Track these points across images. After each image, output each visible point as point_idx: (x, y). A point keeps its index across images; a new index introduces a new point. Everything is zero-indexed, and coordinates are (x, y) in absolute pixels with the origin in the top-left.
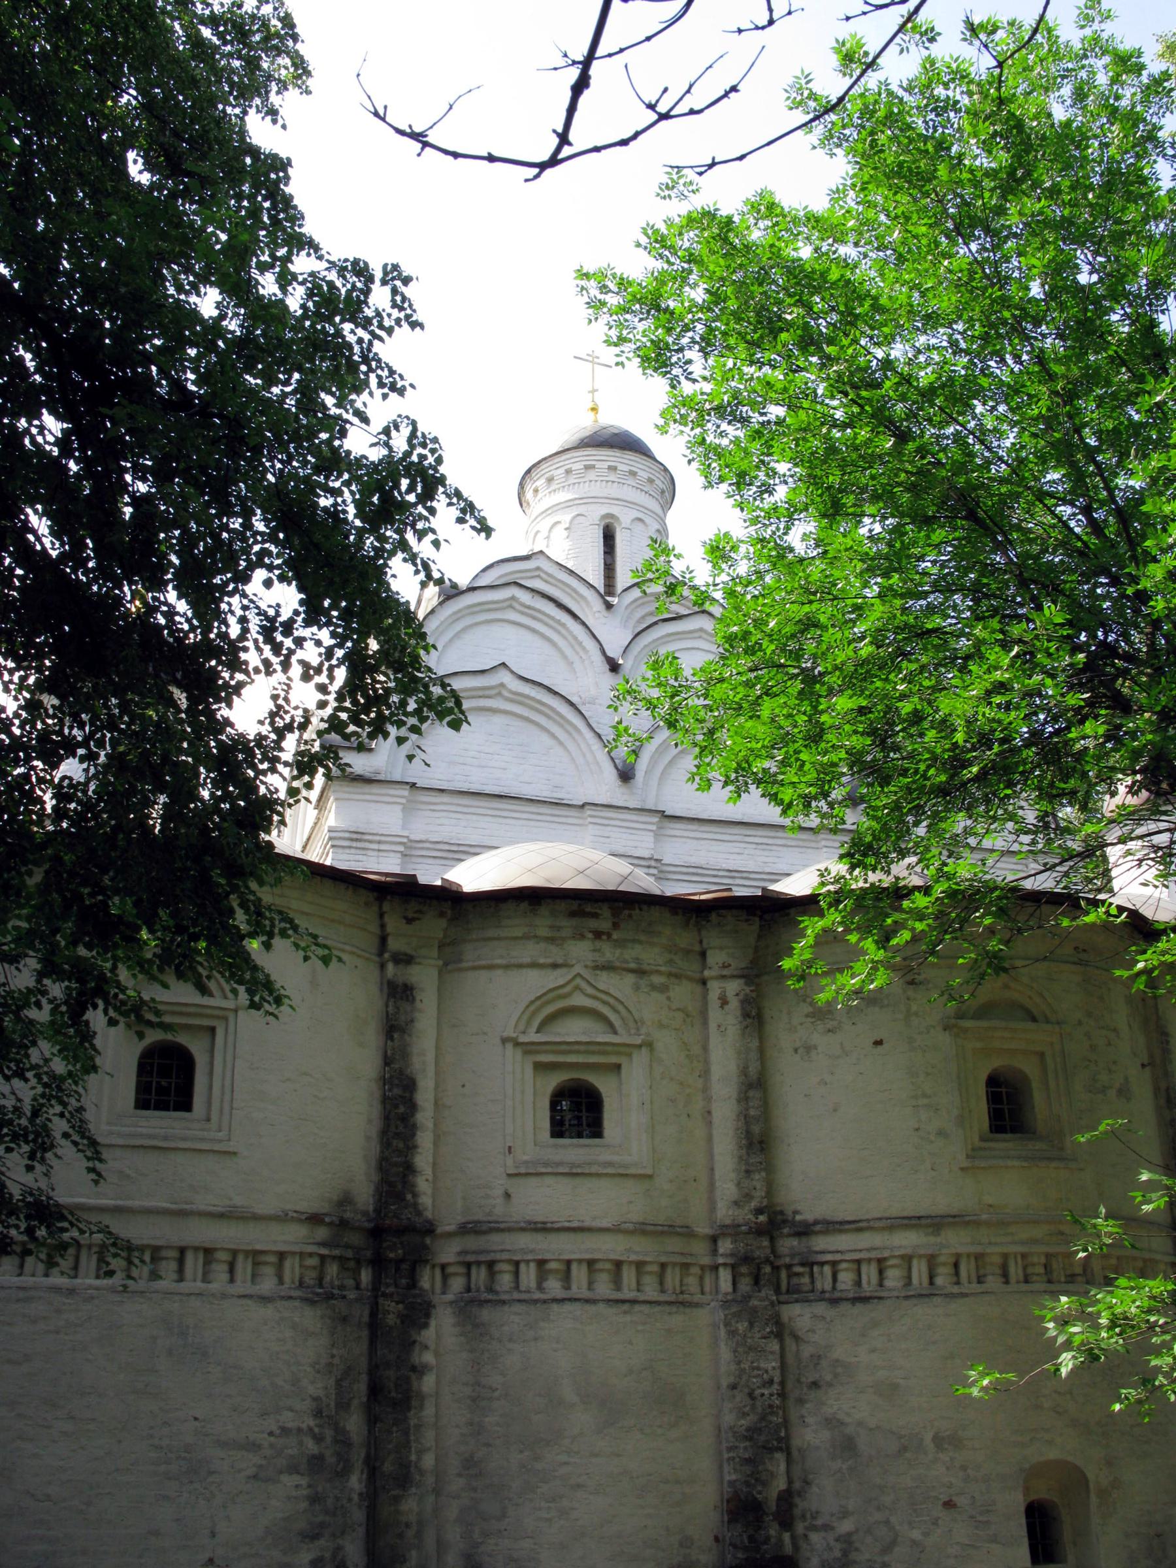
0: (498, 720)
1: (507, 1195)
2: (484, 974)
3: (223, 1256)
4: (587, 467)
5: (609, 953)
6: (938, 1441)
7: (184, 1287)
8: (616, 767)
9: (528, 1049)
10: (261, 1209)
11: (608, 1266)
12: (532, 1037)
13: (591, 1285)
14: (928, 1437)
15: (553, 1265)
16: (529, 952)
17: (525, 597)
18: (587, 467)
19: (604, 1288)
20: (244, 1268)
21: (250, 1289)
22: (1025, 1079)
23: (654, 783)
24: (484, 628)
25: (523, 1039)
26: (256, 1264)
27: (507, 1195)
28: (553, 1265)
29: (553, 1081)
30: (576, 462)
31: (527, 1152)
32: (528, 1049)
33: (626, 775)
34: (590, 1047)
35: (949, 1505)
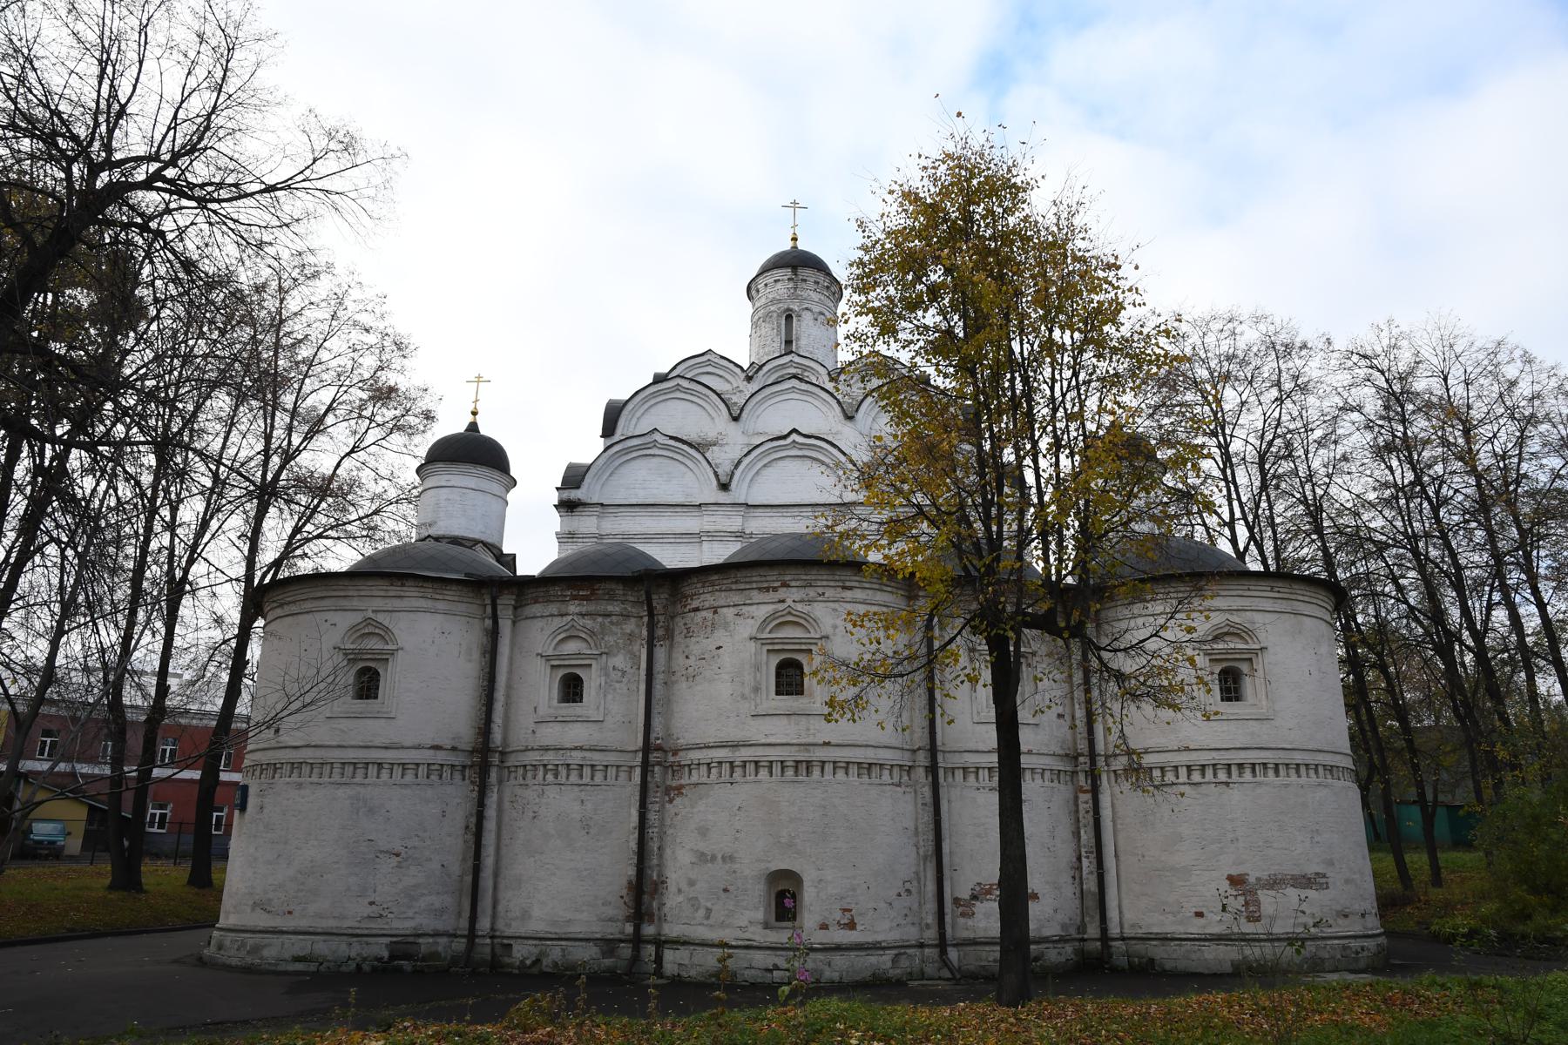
0: (655, 460)
1: (534, 732)
2: (528, 621)
3: (386, 766)
4: (776, 281)
5: (592, 607)
6: (723, 858)
7: (366, 781)
8: (718, 480)
9: (548, 658)
10: (407, 744)
11: (436, 767)
12: (550, 652)
13: (1215, 775)
14: (720, 856)
15: (550, 767)
16: (553, 608)
17: (685, 384)
18: (776, 281)
19: (574, 778)
20: (398, 771)
21: (878, 781)
22: (565, 676)
23: (745, 485)
24: (663, 404)
25: (759, 636)
26: (404, 769)
27: (534, 732)
28: (550, 767)
29: (561, 673)
30: (770, 278)
31: (543, 711)
32: (548, 658)
33: (724, 487)
34: (579, 655)
35: (726, 890)
